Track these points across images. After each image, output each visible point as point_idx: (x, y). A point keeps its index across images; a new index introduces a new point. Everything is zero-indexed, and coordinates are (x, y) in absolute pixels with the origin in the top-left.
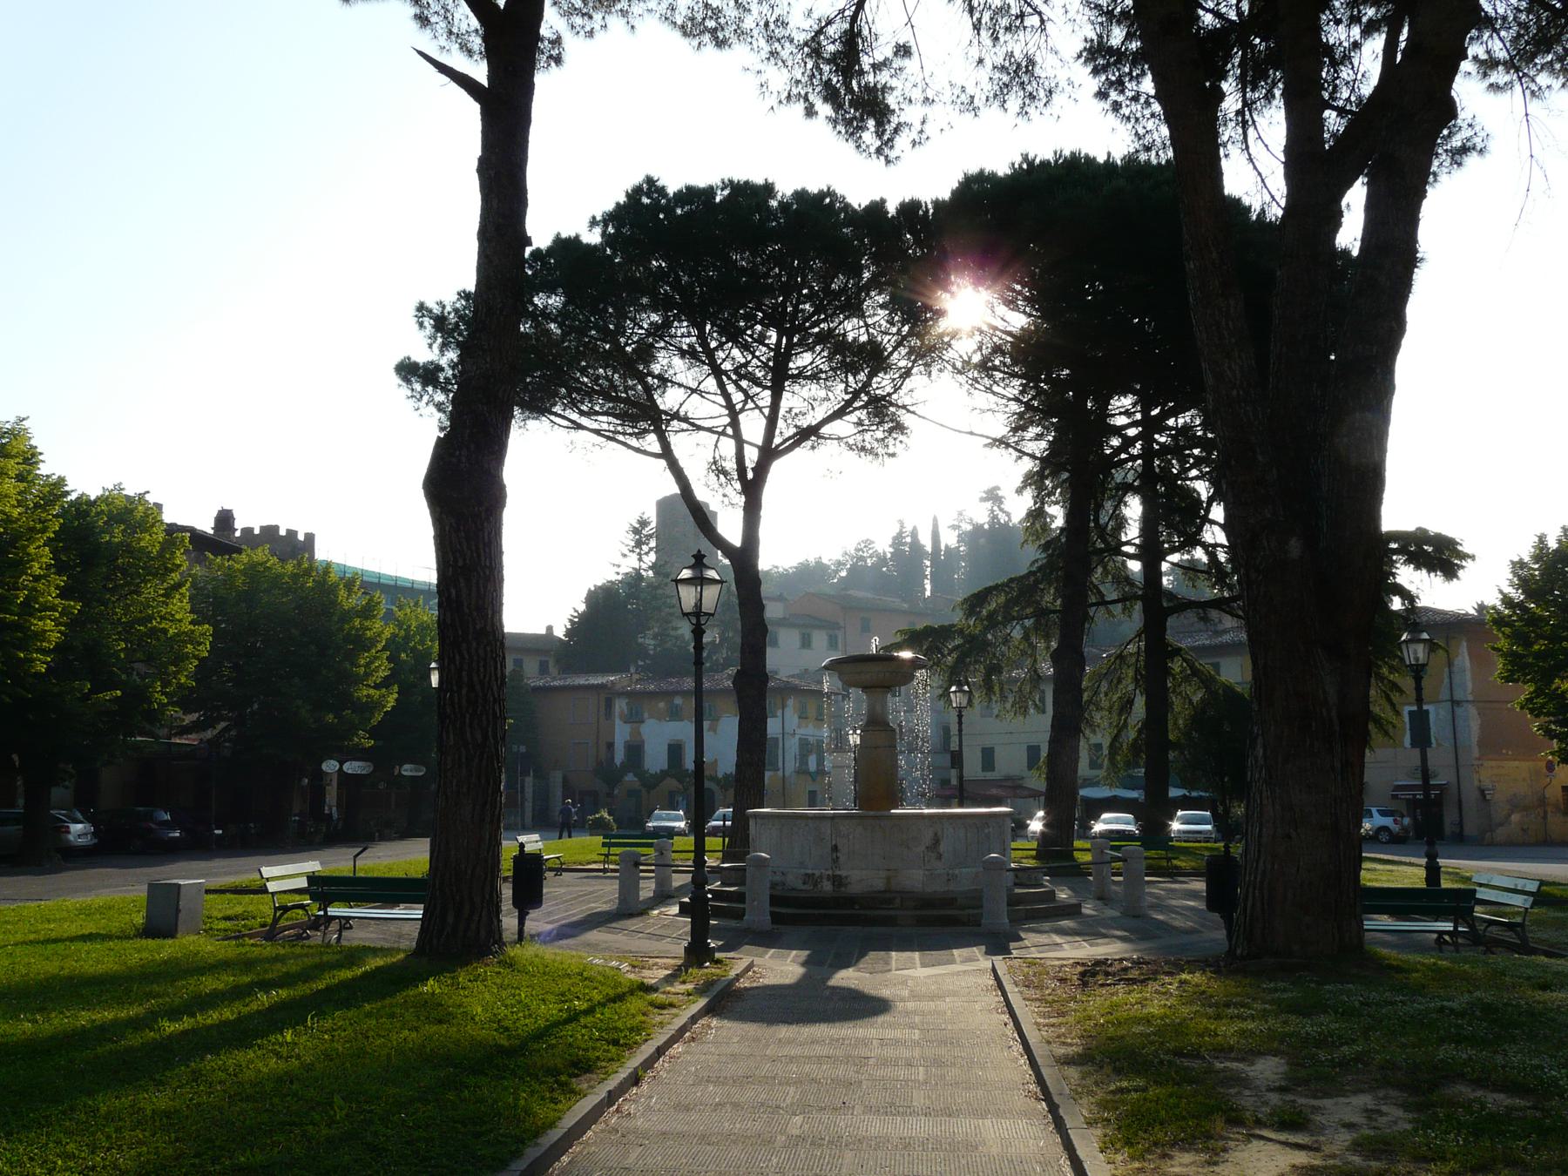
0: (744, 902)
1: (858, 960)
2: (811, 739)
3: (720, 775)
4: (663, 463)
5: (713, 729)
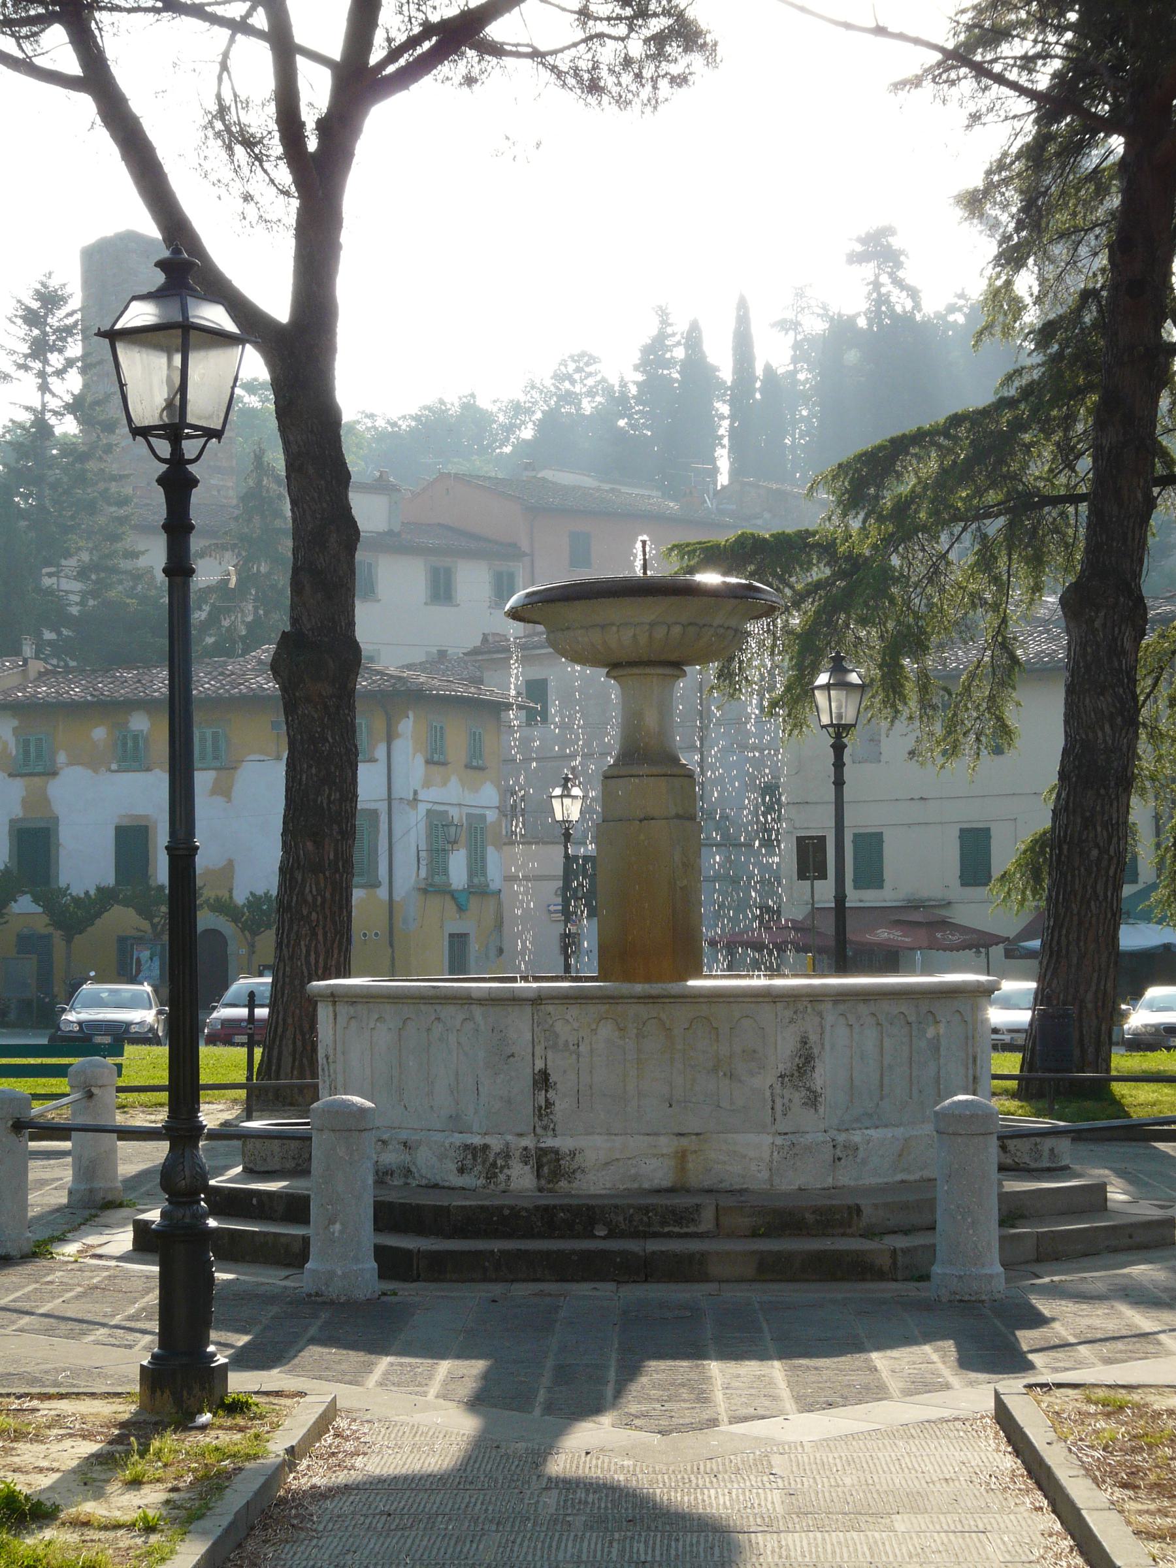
0: (304, 1220)
1: (619, 1393)
2: (454, 812)
3: (240, 898)
4: (85, 104)
5: (223, 790)
